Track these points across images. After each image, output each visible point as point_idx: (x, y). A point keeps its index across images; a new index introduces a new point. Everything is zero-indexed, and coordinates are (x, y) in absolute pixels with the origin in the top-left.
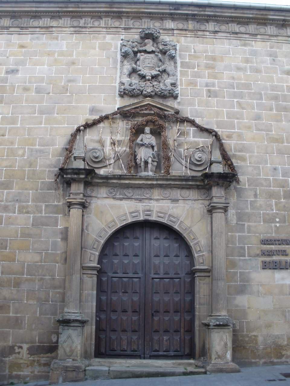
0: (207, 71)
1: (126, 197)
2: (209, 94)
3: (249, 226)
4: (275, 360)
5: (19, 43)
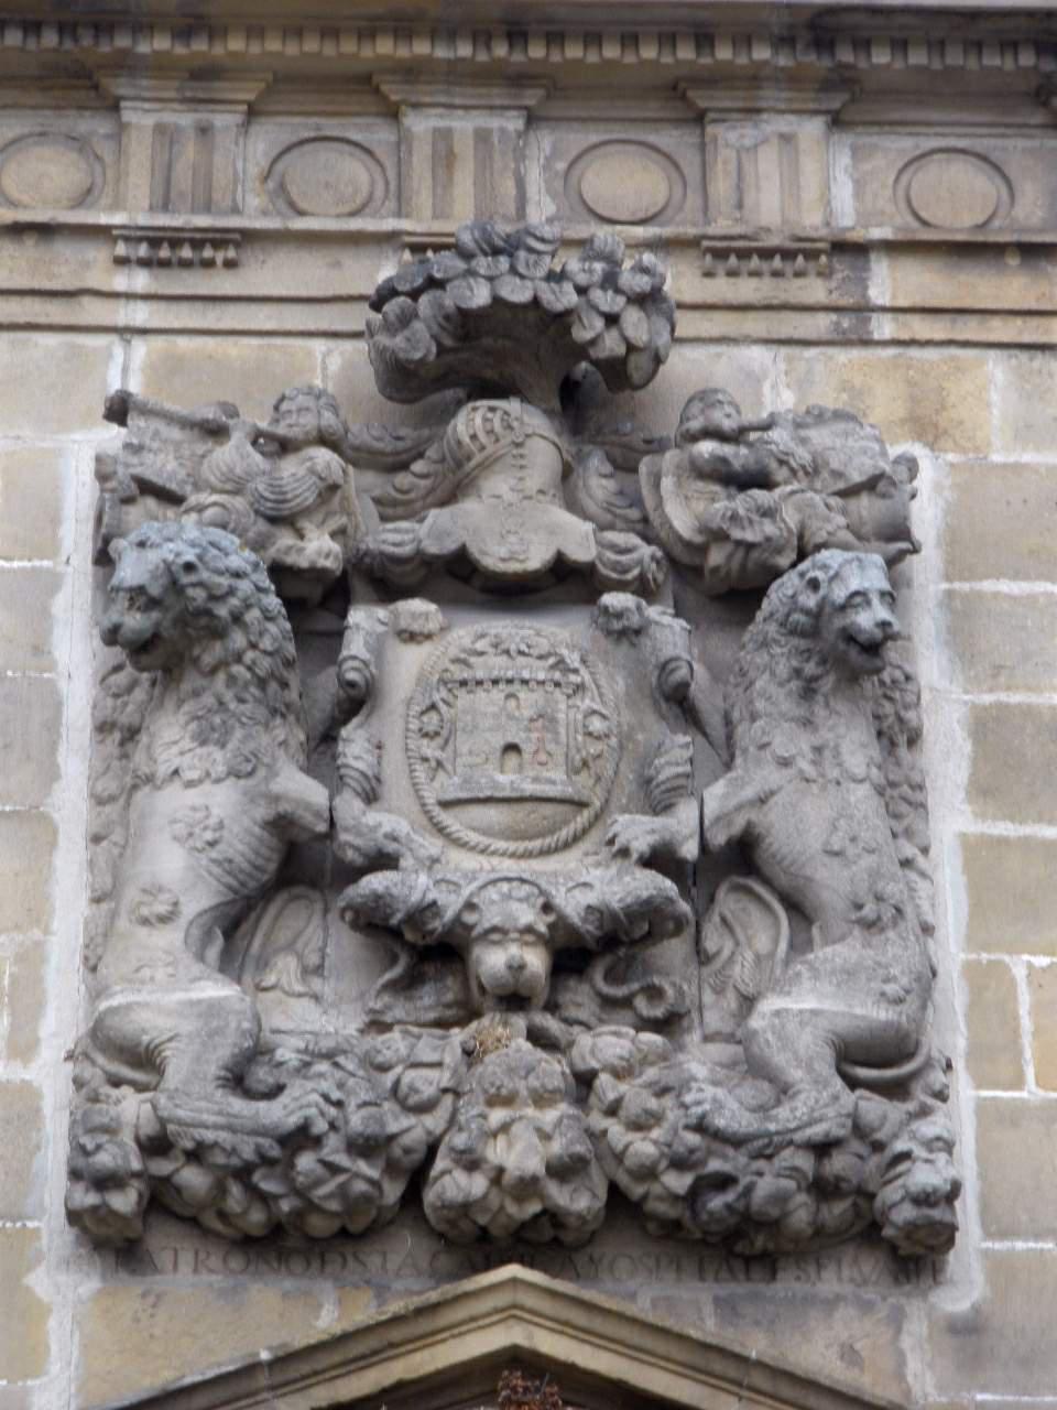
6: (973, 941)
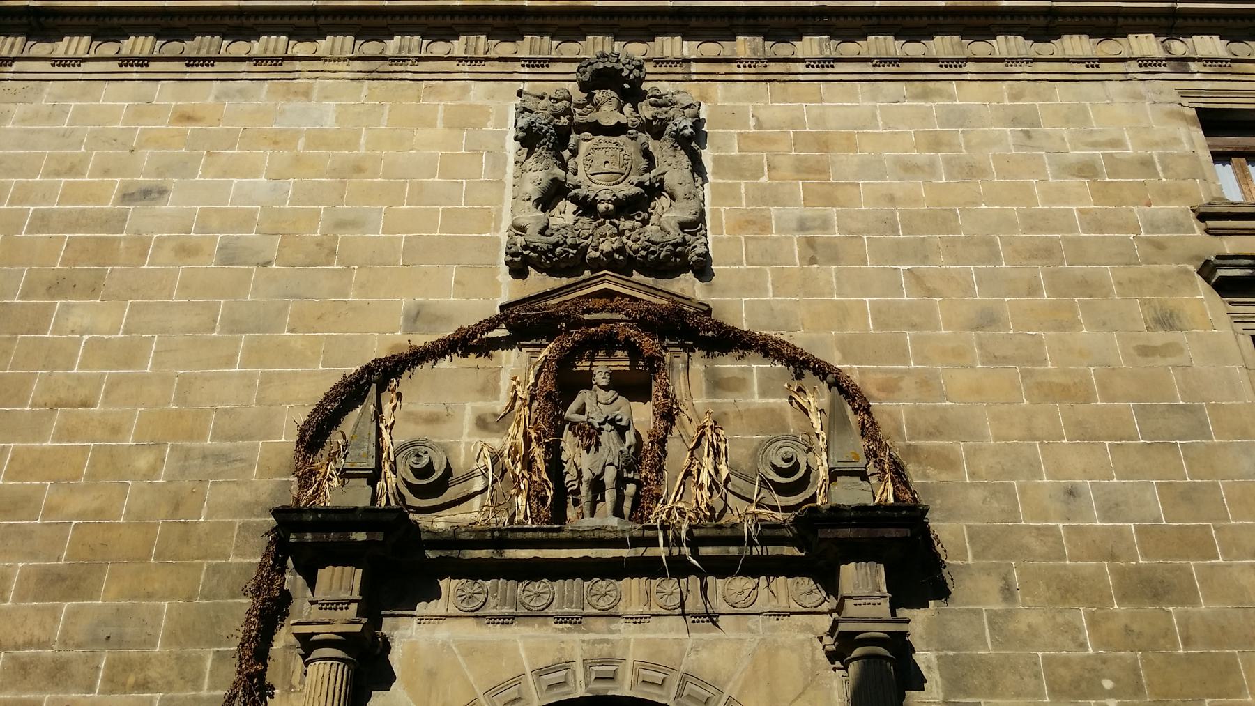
0: (800, 182)
1: (522, 611)
2: (810, 253)
5: (176, 106)
6: (712, 204)
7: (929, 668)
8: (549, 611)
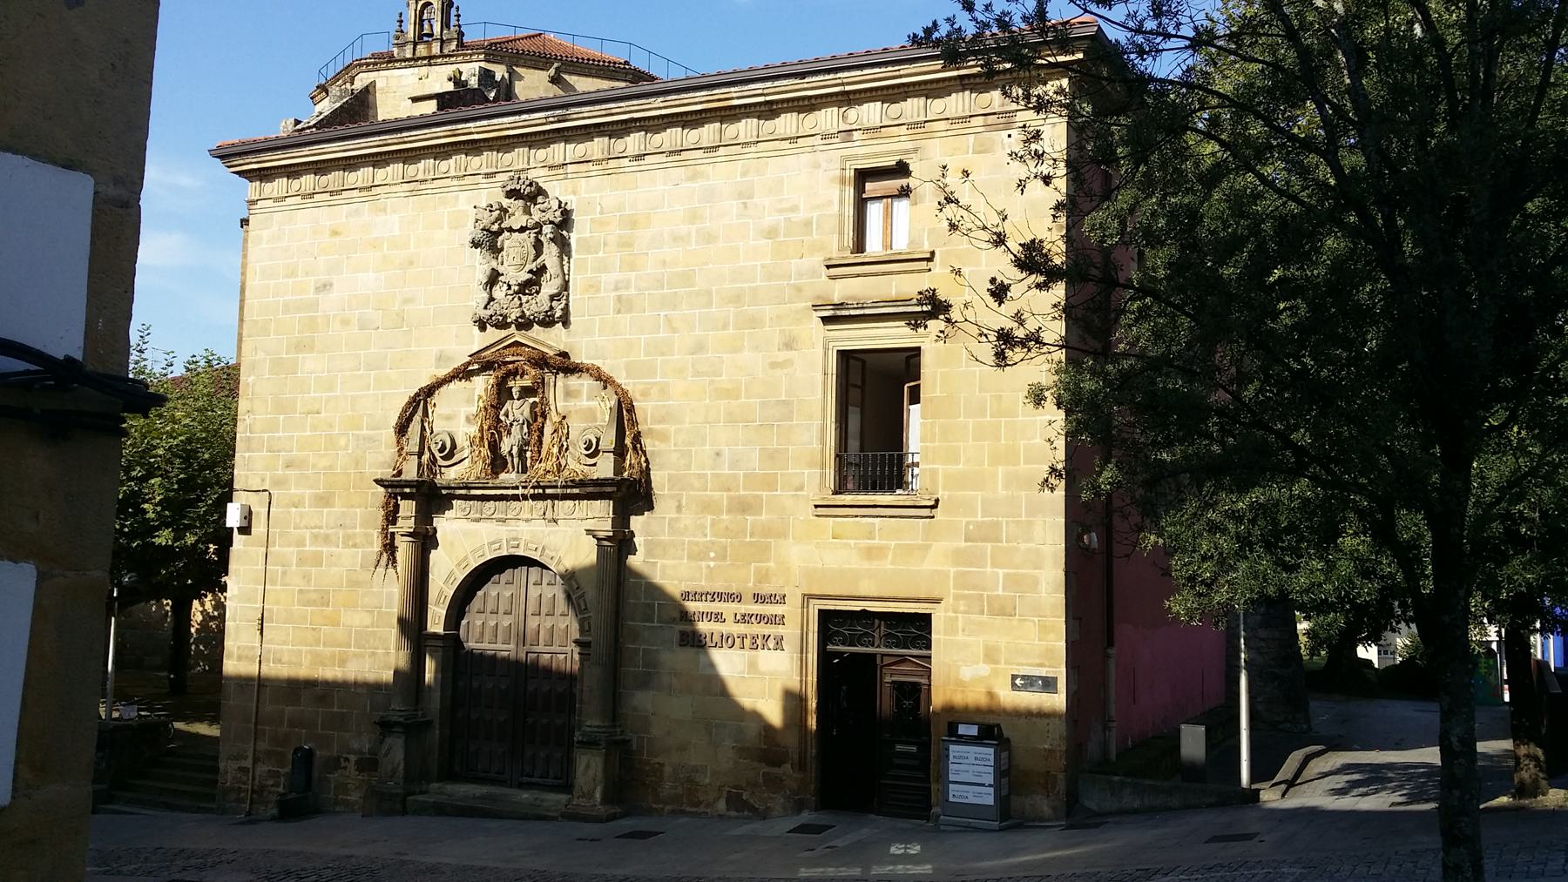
3: (664, 567)
4: (688, 809)
6: (574, 274)
7: (640, 545)
8: (493, 517)
